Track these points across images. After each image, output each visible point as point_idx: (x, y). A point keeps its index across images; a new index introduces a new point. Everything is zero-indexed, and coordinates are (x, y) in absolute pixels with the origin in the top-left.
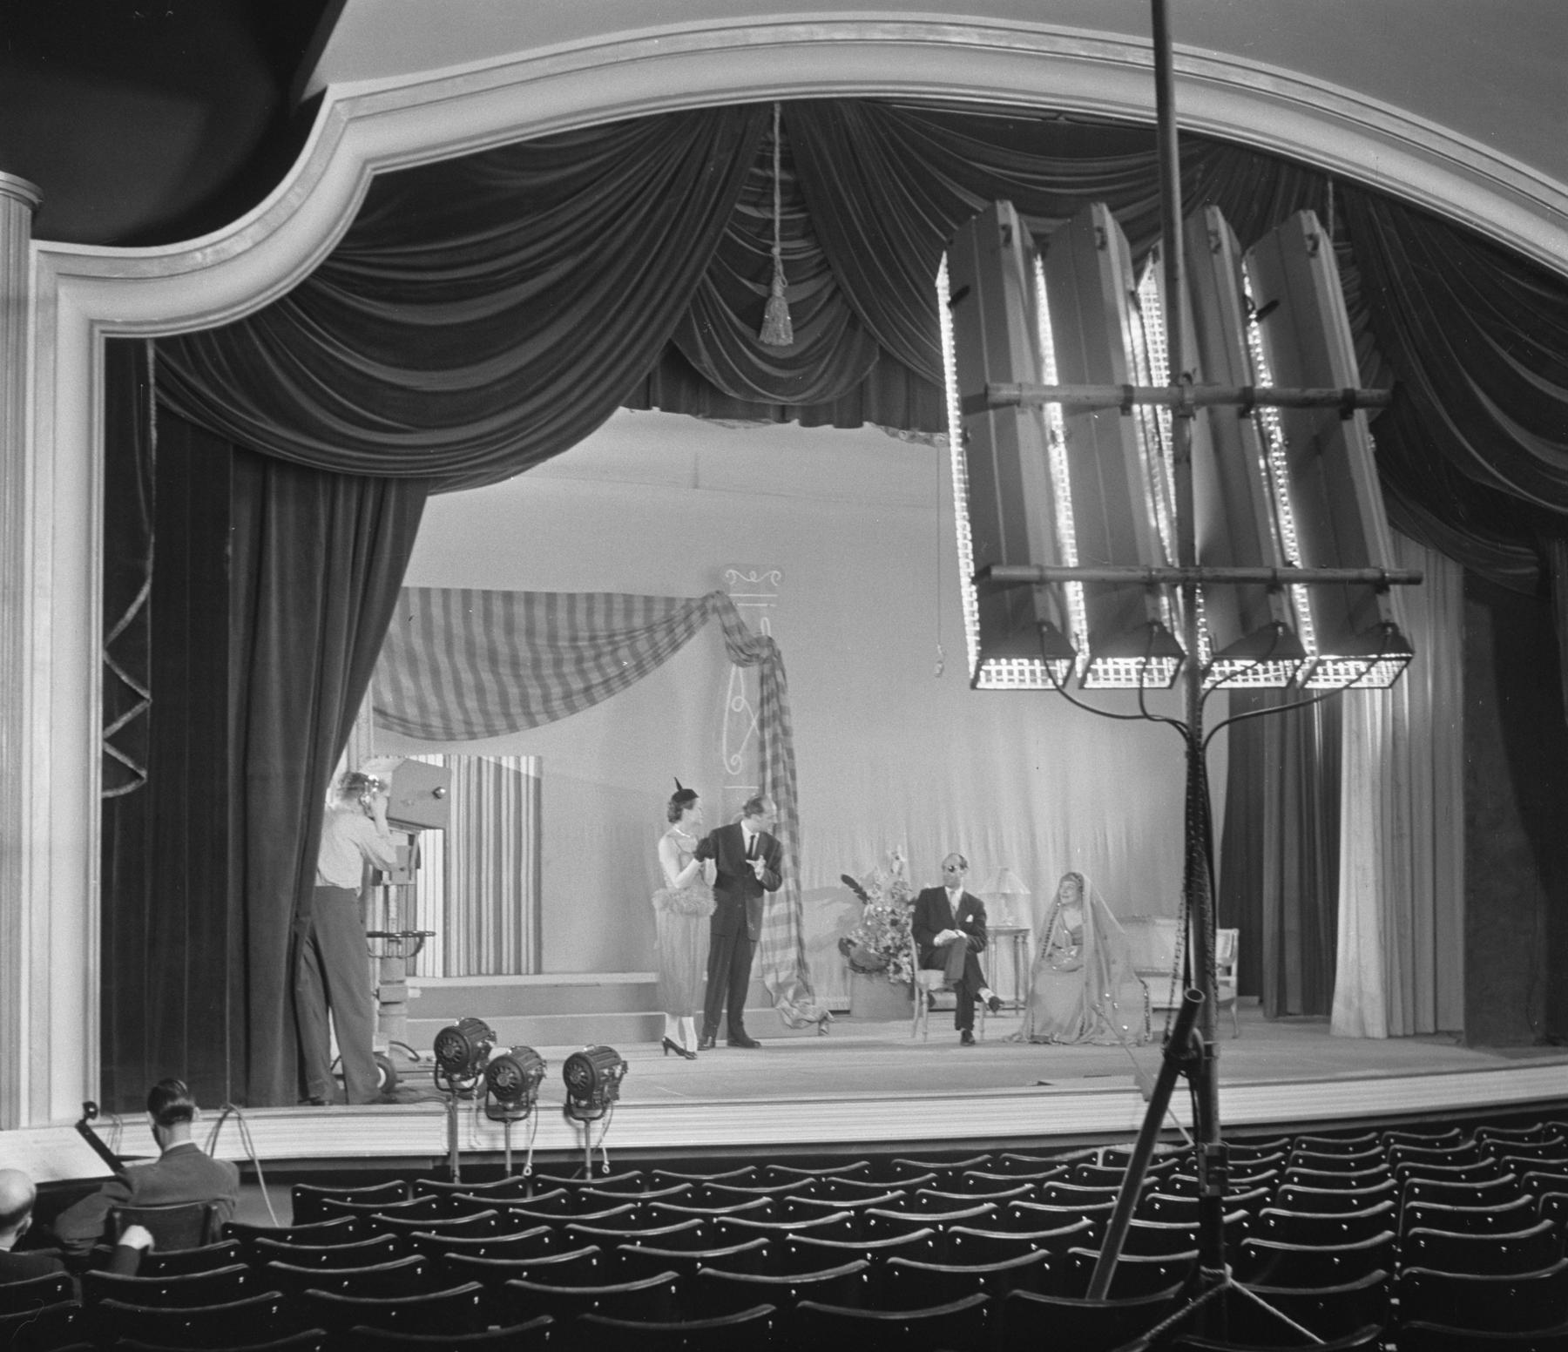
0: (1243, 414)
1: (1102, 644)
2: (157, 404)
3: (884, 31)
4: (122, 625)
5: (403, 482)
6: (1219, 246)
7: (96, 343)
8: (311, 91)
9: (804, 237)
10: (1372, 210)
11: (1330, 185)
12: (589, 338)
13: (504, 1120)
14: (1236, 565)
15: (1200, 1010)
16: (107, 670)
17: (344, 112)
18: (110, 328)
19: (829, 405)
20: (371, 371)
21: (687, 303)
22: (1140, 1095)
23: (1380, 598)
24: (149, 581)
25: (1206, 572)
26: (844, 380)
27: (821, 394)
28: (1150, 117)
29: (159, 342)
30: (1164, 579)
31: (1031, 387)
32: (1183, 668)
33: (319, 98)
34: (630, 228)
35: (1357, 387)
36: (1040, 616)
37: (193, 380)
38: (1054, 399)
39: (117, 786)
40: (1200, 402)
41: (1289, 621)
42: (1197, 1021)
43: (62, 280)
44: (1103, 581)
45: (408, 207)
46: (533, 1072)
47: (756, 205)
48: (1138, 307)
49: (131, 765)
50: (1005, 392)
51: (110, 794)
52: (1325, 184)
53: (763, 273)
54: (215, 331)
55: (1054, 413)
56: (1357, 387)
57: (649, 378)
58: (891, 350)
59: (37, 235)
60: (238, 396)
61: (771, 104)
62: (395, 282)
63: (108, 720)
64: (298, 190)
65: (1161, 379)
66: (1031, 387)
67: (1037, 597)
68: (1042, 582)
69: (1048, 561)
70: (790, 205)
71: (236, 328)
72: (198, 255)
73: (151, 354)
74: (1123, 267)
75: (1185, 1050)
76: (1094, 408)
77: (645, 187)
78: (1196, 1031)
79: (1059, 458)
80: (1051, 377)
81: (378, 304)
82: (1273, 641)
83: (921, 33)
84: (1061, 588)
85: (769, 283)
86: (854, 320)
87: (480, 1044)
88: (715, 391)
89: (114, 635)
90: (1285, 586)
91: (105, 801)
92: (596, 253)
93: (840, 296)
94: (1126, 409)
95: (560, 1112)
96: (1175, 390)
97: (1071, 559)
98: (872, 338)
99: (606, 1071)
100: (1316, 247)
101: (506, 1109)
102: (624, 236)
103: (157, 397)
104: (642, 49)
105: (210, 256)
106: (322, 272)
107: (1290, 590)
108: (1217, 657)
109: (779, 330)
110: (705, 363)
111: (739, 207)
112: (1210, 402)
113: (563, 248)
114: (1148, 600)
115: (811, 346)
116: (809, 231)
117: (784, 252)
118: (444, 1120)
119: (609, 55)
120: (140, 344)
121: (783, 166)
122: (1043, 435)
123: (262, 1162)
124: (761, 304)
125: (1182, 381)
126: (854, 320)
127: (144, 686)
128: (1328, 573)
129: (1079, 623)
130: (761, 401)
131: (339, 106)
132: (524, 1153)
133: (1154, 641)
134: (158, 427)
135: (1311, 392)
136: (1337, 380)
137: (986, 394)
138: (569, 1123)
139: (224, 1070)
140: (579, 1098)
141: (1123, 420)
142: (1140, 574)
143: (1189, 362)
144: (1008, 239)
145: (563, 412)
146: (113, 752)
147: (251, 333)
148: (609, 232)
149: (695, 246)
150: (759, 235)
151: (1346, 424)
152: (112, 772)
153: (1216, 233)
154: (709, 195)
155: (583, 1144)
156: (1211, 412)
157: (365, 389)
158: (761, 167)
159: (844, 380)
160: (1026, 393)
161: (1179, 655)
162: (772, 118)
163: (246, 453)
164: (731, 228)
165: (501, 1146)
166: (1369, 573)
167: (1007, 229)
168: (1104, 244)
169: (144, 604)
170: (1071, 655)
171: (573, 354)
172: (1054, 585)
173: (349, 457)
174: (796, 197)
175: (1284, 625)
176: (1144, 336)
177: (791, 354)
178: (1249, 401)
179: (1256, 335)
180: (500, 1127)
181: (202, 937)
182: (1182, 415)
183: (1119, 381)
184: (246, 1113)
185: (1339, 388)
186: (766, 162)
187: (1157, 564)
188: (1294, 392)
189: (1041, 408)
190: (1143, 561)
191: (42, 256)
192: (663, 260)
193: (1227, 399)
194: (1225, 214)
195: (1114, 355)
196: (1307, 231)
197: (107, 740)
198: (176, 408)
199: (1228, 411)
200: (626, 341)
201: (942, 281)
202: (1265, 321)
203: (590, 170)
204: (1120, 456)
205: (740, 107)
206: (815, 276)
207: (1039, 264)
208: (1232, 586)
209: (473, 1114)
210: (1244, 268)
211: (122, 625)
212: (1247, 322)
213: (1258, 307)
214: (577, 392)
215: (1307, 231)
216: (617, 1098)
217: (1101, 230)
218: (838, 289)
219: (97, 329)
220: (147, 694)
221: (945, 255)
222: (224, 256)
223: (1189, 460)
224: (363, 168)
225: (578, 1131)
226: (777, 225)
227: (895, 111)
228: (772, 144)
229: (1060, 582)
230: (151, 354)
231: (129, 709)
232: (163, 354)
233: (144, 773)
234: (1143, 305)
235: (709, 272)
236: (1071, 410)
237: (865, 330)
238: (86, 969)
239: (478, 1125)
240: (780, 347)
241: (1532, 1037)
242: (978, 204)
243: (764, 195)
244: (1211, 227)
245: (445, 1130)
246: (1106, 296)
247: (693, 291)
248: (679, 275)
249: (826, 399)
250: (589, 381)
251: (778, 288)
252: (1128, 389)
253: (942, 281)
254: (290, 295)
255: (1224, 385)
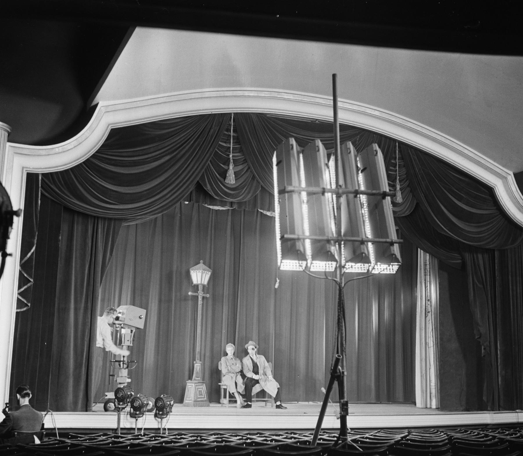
0: (356, 196)
1: (314, 258)
2: (41, 193)
3: (265, 94)
4: (26, 258)
5: (115, 219)
6: (350, 152)
7: (24, 174)
8: (94, 103)
9: (239, 152)
10: (410, 151)
11: (397, 144)
12: (173, 179)
13: (135, 418)
14: (352, 236)
15: (340, 361)
16: (20, 272)
17: (103, 110)
18: (28, 169)
19: (245, 202)
20: (106, 186)
21: (203, 170)
22: (335, 417)
23: (392, 247)
24: (35, 246)
25: (344, 238)
26: (250, 195)
27: (243, 199)
28: (332, 119)
29: (43, 174)
30: (333, 240)
31: (297, 187)
32: (338, 266)
33: (97, 105)
34: (187, 148)
35: (388, 191)
36: (297, 248)
37: (52, 186)
38: (304, 190)
39: (21, 308)
40: (344, 193)
41: (366, 252)
42: (340, 364)
43: (15, 155)
44: (315, 240)
45: (121, 138)
46: (145, 402)
47: (225, 143)
48: (328, 167)
49: (25, 302)
50: (289, 188)
51: (19, 310)
52: (396, 143)
53: (227, 162)
54: (60, 172)
55: (304, 195)
56: (388, 191)
57: (191, 192)
58: (265, 187)
59: (9, 141)
60: (66, 192)
61: (231, 113)
62: (116, 160)
63: (19, 288)
64: (88, 131)
65: (334, 186)
66: (297, 187)
67: (297, 243)
68: (299, 239)
69: (300, 233)
70: (236, 143)
71: (66, 171)
72: (57, 149)
73: (40, 178)
74: (324, 157)
75: (337, 372)
76: (314, 194)
77: (190, 138)
78: (340, 367)
79: (305, 208)
80: (303, 184)
81: (111, 167)
82: (364, 259)
83: (275, 95)
84: (304, 241)
85: (228, 165)
86: (254, 177)
87: (129, 393)
88: (211, 197)
89: (23, 261)
90: (366, 243)
91: (17, 313)
92: (177, 154)
93: (249, 170)
94: (323, 193)
95: (153, 416)
96: (337, 190)
97: (307, 233)
98: (259, 183)
99: (168, 403)
100: (377, 153)
101: (136, 414)
102: (185, 150)
103: (41, 191)
104: (193, 96)
105: (61, 149)
106: (94, 156)
107: (367, 244)
108: (347, 262)
109: (231, 179)
110: (208, 188)
111: (220, 143)
112: (347, 193)
113: (167, 152)
114: (328, 245)
115: (241, 184)
116: (241, 151)
117: (233, 156)
118: (116, 417)
119: (183, 97)
120: (37, 175)
121: (234, 131)
122: (301, 201)
123: (58, 429)
124: (226, 171)
125: (339, 187)
126: (254, 177)
127: (31, 278)
128: (377, 240)
129: (309, 252)
130: (225, 200)
131: (102, 108)
132: (141, 429)
133: (330, 257)
134: (41, 199)
135: (374, 192)
136: (381, 188)
137: (285, 189)
138: (156, 420)
139: (47, 400)
140: (159, 411)
141: (322, 197)
142: (325, 238)
143: (341, 182)
144: (292, 148)
145: (164, 201)
146: (20, 298)
147: (71, 173)
148: (181, 148)
149: (207, 153)
150: (226, 151)
151: (384, 201)
152: (20, 304)
153: (349, 149)
154: (211, 139)
155: (160, 427)
156: (347, 196)
157: (105, 191)
158: (227, 132)
159: (250, 195)
160: (296, 189)
161: (336, 261)
162: (231, 117)
163: (68, 210)
164: (218, 149)
165: (134, 426)
166: (388, 240)
167: (292, 145)
168: (319, 150)
169: (33, 252)
170: (306, 260)
171: (169, 183)
172: (302, 240)
173: (99, 211)
174: (237, 141)
175: (365, 254)
176: (329, 176)
177: (234, 186)
178: (357, 193)
179: (361, 177)
180: (134, 420)
181: (46, 355)
182: (339, 196)
183: (321, 187)
184: (54, 413)
185: (382, 191)
186: (229, 130)
187: (330, 235)
188: (369, 191)
189: (300, 193)
190: (327, 235)
191: (10, 148)
192: (198, 156)
193: (351, 193)
194: (353, 144)
195: (320, 179)
196: (374, 149)
197: (19, 294)
198: (47, 194)
199: (351, 196)
200: (185, 181)
201: (275, 160)
202: (363, 173)
203: (176, 130)
204: (321, 209)
205: (222, 114)
206: (242, 164)
207: (301, 155)
208: (351, 242)
209: (126, 416)
210: (358, 159)
211: (26, 258)
212: (358, 173)
213: (362, 169)
214: (169, 195)
215: (374, 149)
216: (171, 412)
217: (318, 146)
218: (249, 168)
219: (25, 170)
220: (32, 280)
221: (275, 152)
222: (65, 150)
223: (340, 209)
224: (108, 127)
225: (159, 422)
226: (231, 148)
227: (268, 117)
228: (230, 125)
229: (304, 239)
230: (40, 178)
231: (26, 284)
232: (45, 179)
233: (29, 305)
234: (330, 168)
235: (210, 161)
236: (309, 194)
237: (257, 181)
238: (7, 365)
239: (127, 419)
240: (231, 185)
241: (462, 408)
242: (284, 139)
243: (228, 140)
244: (348, 147)
245: (116, 420)
246: (319, 164)
247: (206, 167)
248: (203, 159)
249: (245, 200)
250: (173, 192)
251: (231, 167)
252: (324, 189)
253: (275, 160)
254: (84, 162)
255: (350, 189)
